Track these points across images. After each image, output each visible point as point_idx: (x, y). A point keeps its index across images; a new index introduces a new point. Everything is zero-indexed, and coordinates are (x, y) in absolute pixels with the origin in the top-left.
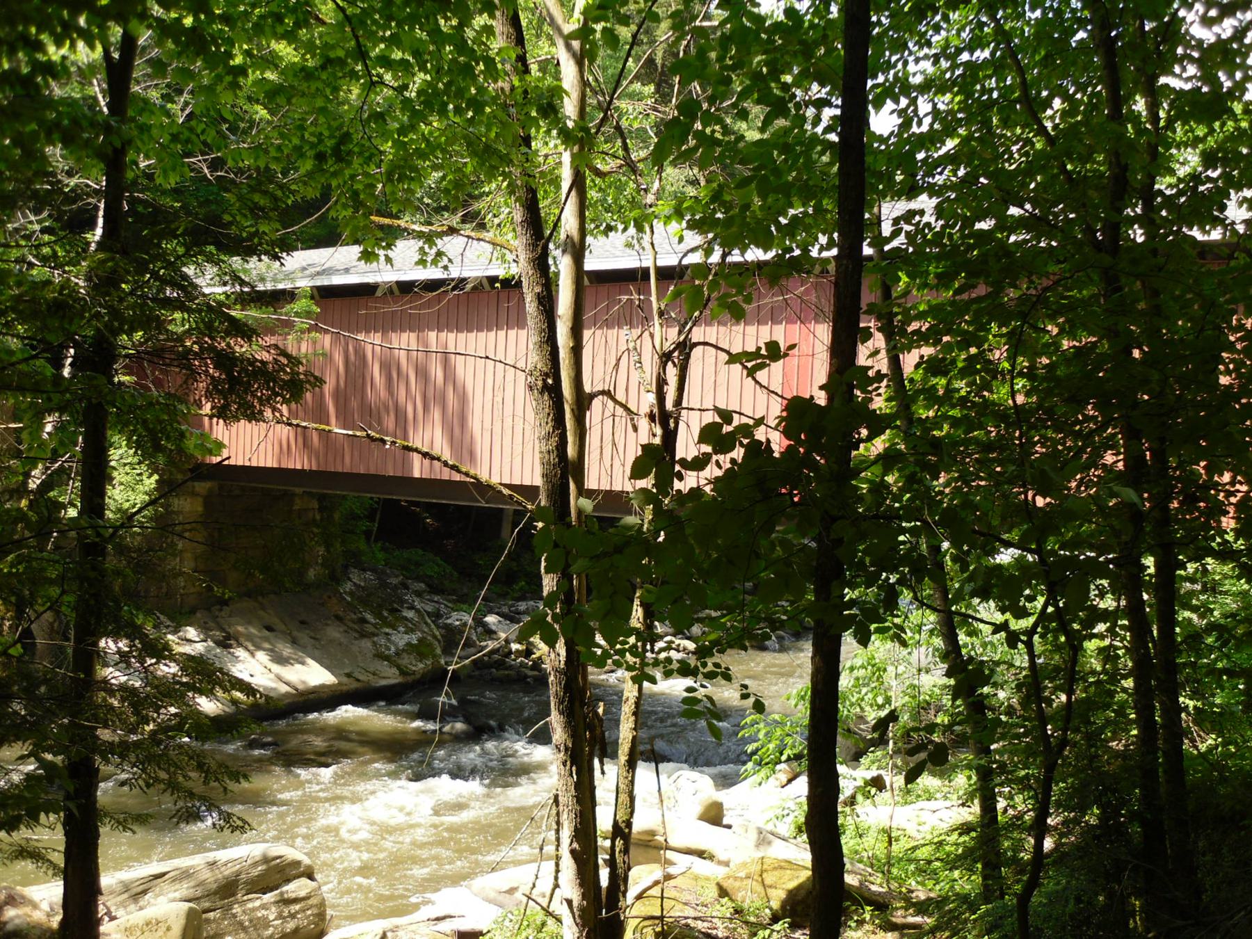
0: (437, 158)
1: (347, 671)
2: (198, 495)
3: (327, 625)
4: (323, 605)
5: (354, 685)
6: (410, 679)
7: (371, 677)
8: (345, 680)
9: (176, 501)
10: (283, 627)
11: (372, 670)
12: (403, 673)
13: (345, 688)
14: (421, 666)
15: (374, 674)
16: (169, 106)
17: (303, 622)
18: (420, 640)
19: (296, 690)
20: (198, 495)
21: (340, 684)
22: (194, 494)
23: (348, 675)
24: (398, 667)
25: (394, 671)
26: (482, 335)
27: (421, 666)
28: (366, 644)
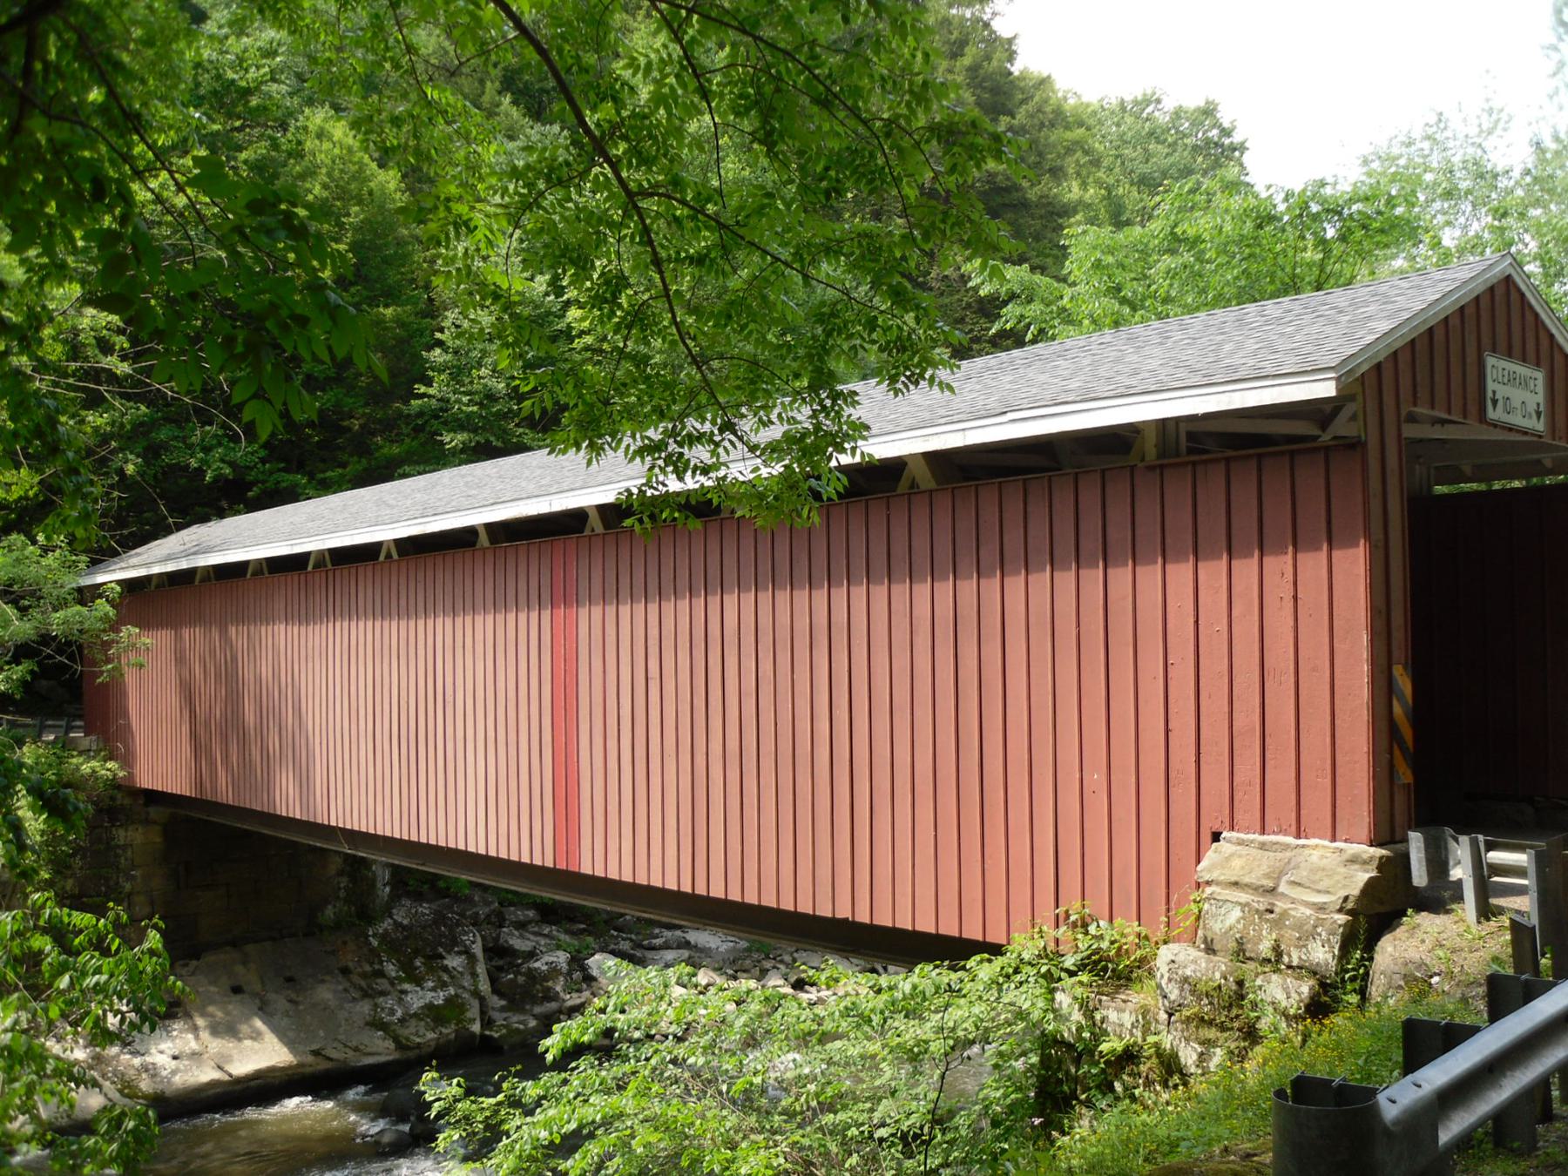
0: (763, 354)
1: (315, 1047)
2: (155, 822)
3: (323, 981)
4: (333, 953)
5: (323, 1065)
6: (411, 1054)
7: (351, 1053)
8: (310, 1059)
9: (122, 833)
10: (258, 987)
11: (354, 1043)
12: (400, 1046)
13: (308, 1070)
14: (431, 1035)
15: (356, 1049)
16: (1559, 190)
17: (290, 980)
18: (448, 1000)
19: (231, 1075)
20: (155, 822)
21: (300, 1065)
22: (147, 822)
23: (316, 1053)
24: (396, 1039)
25: (390, 1044)
26: (341, 626)
27: (431, 1035)
28: (365, 1008)
